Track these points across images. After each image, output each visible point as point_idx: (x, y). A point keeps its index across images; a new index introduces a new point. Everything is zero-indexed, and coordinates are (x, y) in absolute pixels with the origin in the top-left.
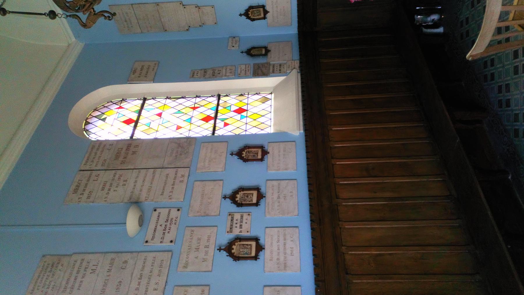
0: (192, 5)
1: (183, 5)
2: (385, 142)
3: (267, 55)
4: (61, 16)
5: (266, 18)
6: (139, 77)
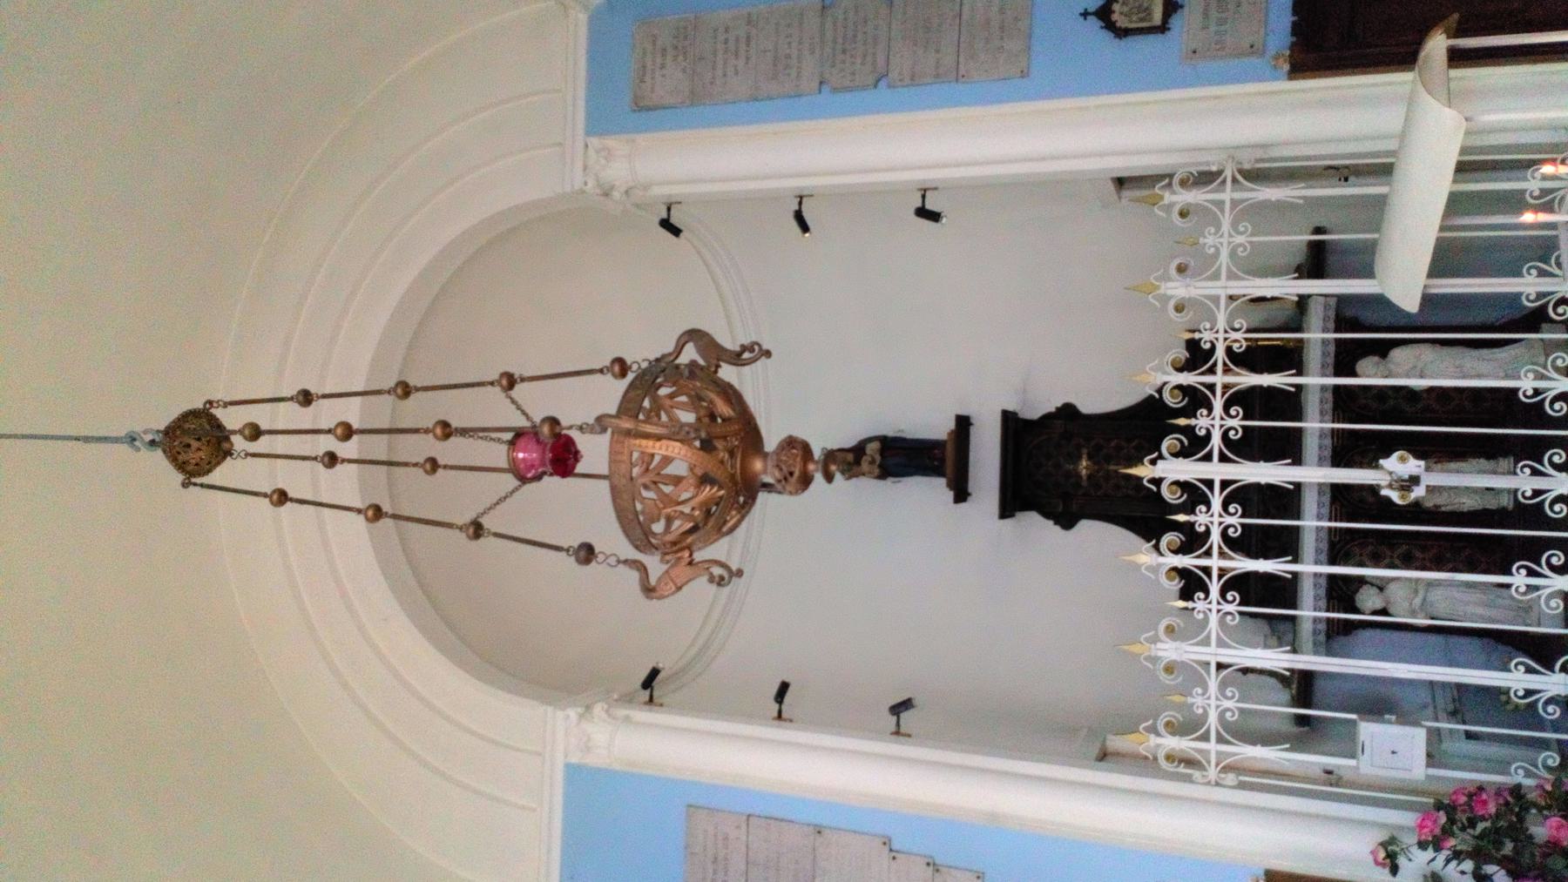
1: (891, 850)
2: (1490, 237)
4: (605, 560)
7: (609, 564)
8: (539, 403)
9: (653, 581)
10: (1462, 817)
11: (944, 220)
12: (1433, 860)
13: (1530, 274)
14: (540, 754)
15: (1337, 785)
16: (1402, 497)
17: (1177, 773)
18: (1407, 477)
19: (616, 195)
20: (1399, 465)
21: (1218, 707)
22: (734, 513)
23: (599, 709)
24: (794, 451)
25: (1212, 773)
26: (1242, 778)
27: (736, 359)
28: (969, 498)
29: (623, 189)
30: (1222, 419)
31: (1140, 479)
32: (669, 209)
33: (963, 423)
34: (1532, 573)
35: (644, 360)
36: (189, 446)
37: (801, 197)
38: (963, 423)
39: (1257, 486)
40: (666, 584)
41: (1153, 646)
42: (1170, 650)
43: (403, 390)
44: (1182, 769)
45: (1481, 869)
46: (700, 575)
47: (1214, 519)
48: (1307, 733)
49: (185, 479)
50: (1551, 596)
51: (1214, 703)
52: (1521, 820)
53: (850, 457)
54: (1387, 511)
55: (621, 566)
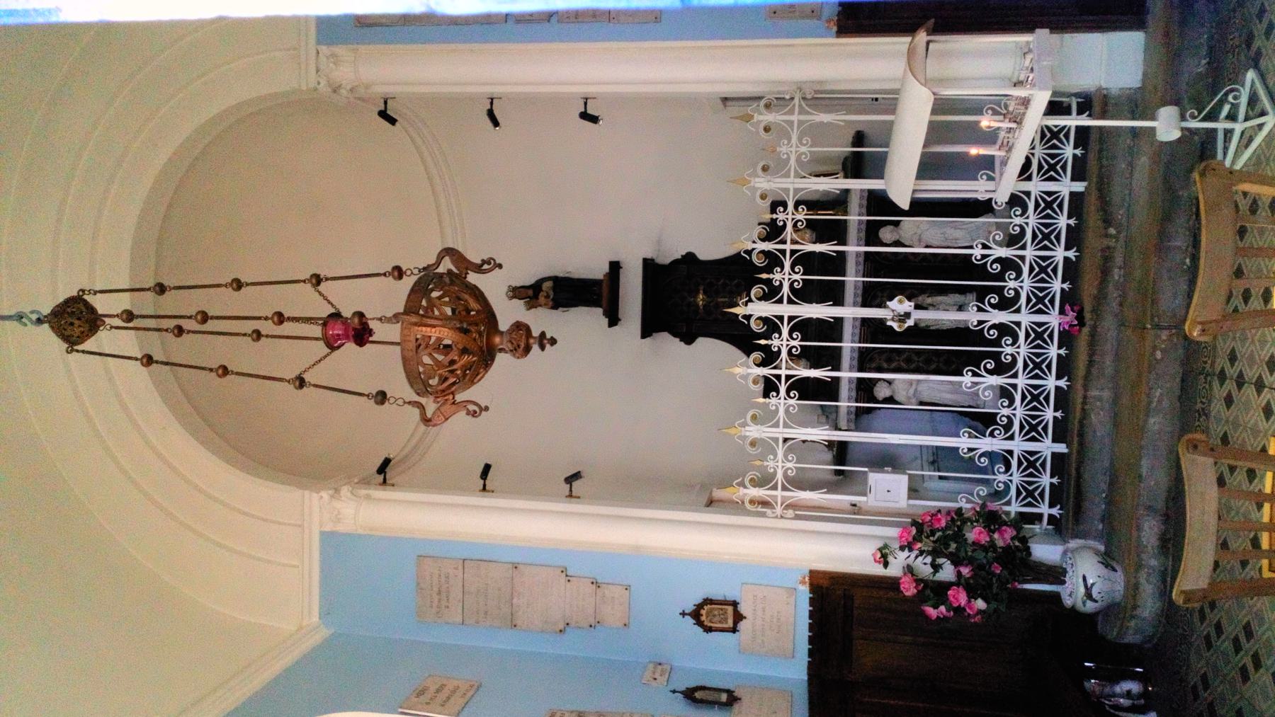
0: (585, 578)
1: (567, 576)
3: (732, 705)
5: (738, 631)
6: (427, 703)
7: (397, 404)
8: (349, 299)
9: (429, 415)
10: (927, 529)
11: (601, 122)
12: (909, 557)
13: (982, 179)
14: (300, 526)
15: (858, 514)
16: (900, 327)
17: (758, 511)
18: (902, 313)
19: (343, 92)
20: (900, 305)
21: (783, 467)
22: (482, 370)
23: (345, 491)
24: (521, 332)
25: (779, 510)
26: (797, 512)
27: (478, 269)
28: (620, 322)
29: (348, 88)
30: (790, 274)
31: (737, 315)
32: (386, 103)
33: (615, 267)
34: (975, 374)
35: (414, 268)
36: (72, 324)
37: (492, 99)
38: (615, 267)
39: (810, 320)
40: (438, 416)
41: (743, 429)
42: (754, 431)
43: (237, 285)
44: (760, 509)
45: (935, 561)
46: (461, 411)
47: (783, 342)
48: (842, 480)
49: (68, 348)
50: (985, 389)
51: (781, 465)
52: (960, 529)
53: (530, 292)
54: (890, 335)
55: (406, 405)
